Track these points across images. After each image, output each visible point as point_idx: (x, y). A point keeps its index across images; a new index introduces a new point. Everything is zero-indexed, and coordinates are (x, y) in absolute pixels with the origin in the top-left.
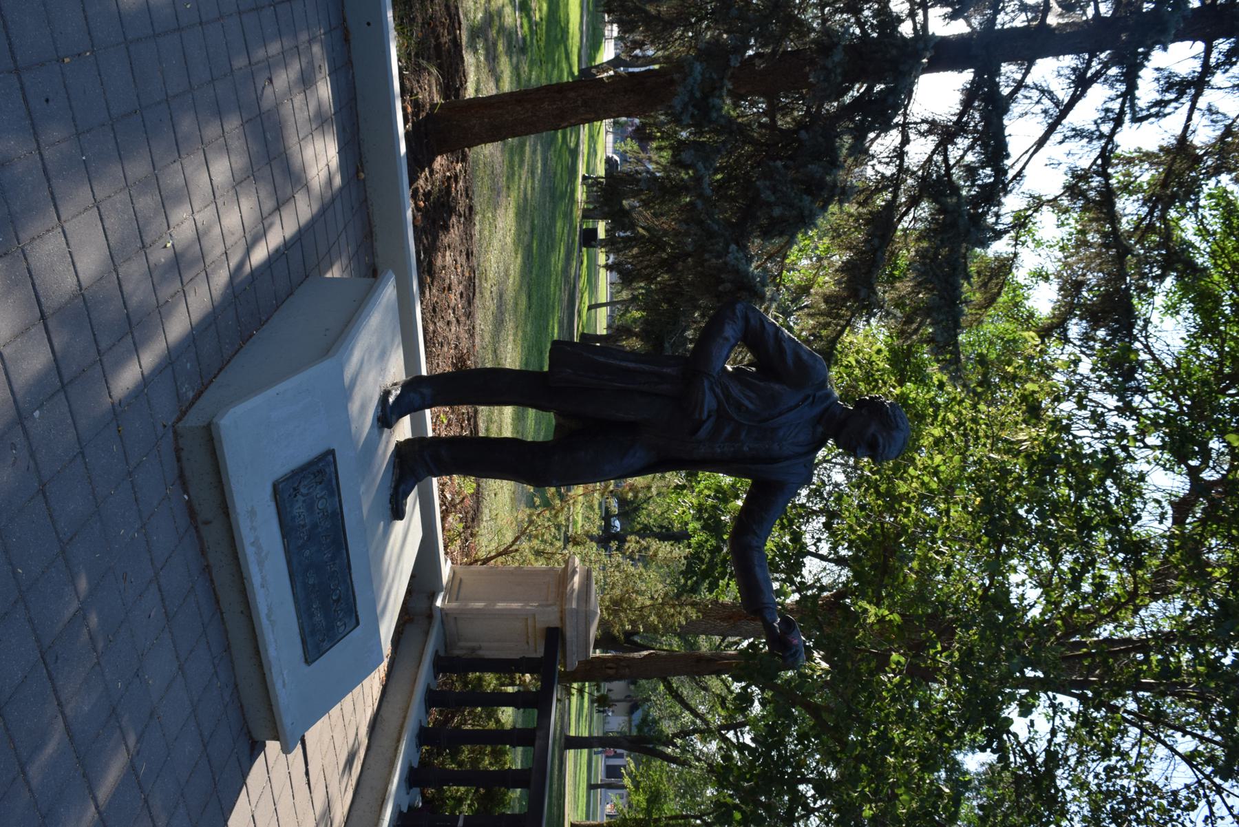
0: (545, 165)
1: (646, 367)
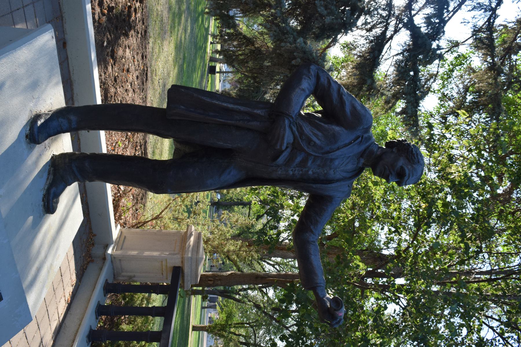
0: (192, 29)
1: (242, 108)
